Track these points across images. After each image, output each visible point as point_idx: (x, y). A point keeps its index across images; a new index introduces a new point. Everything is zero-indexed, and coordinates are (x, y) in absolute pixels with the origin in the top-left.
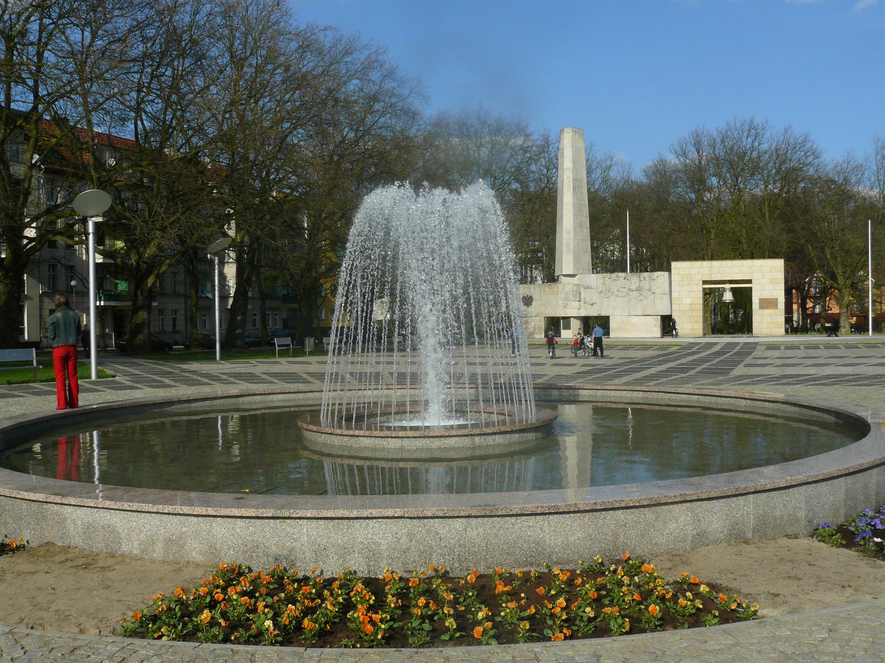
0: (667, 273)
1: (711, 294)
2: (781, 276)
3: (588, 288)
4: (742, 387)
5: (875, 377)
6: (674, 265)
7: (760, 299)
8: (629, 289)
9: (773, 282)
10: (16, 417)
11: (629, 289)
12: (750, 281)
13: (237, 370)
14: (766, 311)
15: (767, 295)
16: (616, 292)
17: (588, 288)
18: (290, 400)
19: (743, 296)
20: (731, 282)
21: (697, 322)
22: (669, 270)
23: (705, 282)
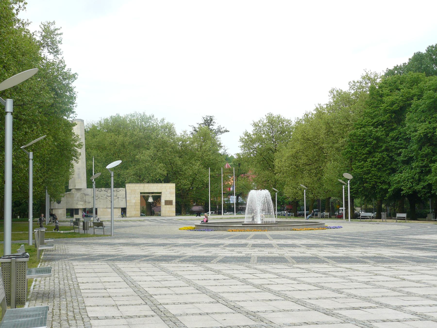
0: (124, 189)
1: (144, 197)
2: (174, 191)
3: (87, 195)
4: (173, 243)
5: (178, 238)
6: (127, 185)
7: (165, 201)
8: (107, 196)
9: (170, 193)
10: (79, 244)
11: (107, 196)
12: (160, 193)
13: (285, 240)
14: (167, 206)
15: (168, 199)
16: (100, 197)
17: (87, 195)
18: (278, 230)
19: (157, 197)
20: (152, 193)
21: (137, 211)
22: (125, 187)
23: (141, 193)
